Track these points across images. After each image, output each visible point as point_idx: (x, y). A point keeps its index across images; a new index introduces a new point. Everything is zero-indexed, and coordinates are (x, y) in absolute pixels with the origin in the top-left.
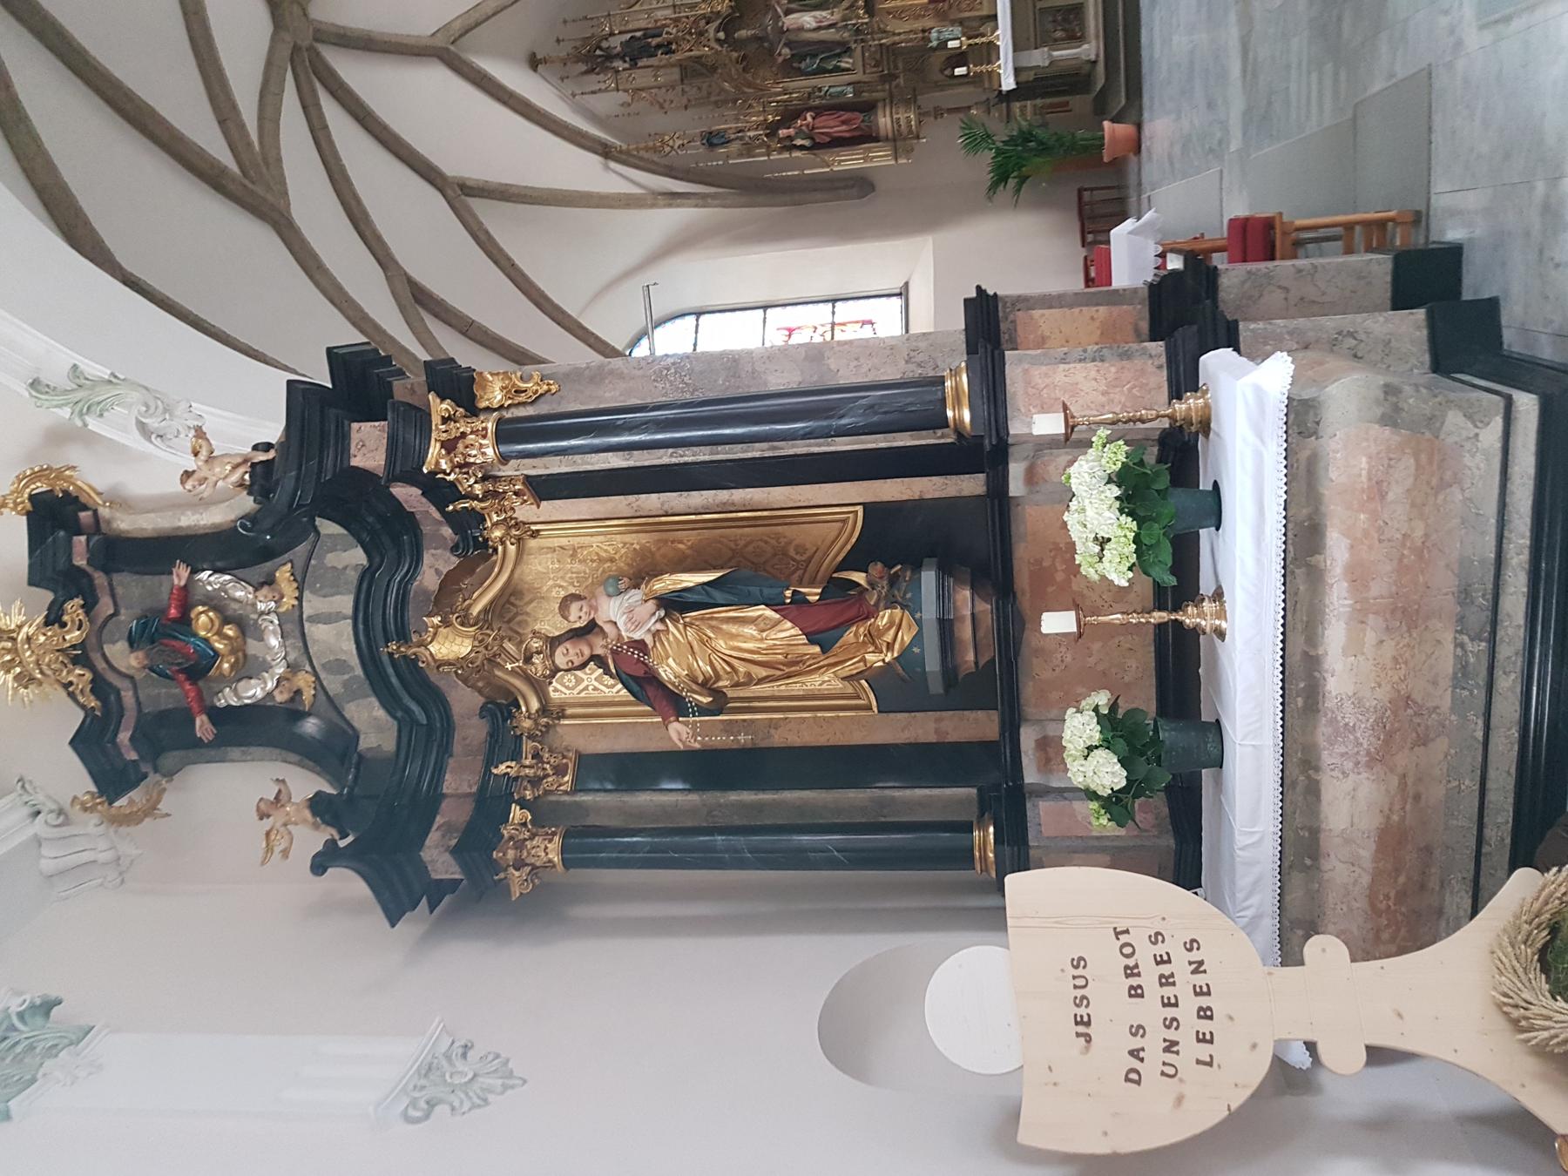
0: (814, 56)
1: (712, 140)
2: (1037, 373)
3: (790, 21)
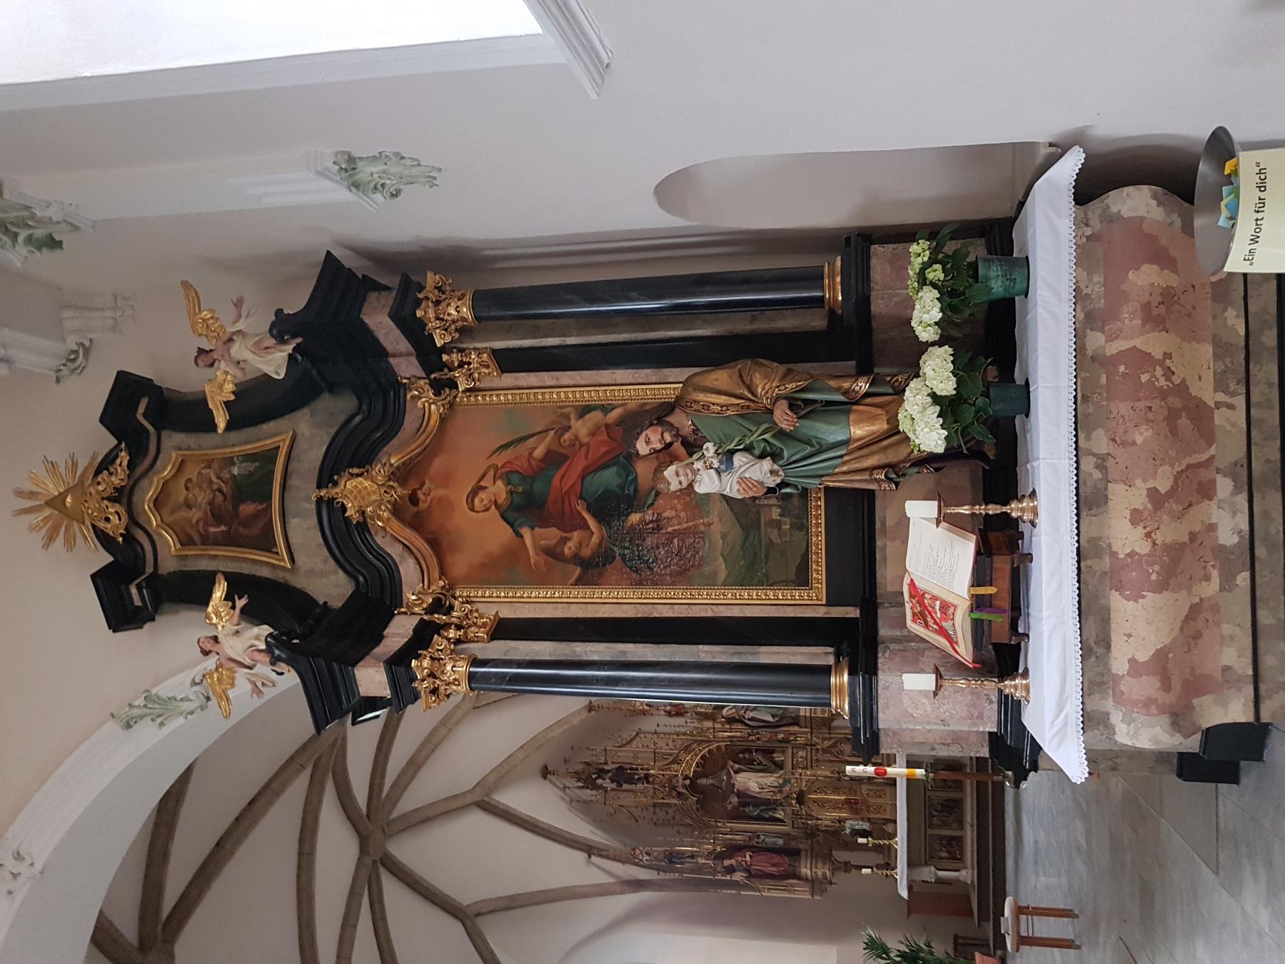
0: (756, 806)
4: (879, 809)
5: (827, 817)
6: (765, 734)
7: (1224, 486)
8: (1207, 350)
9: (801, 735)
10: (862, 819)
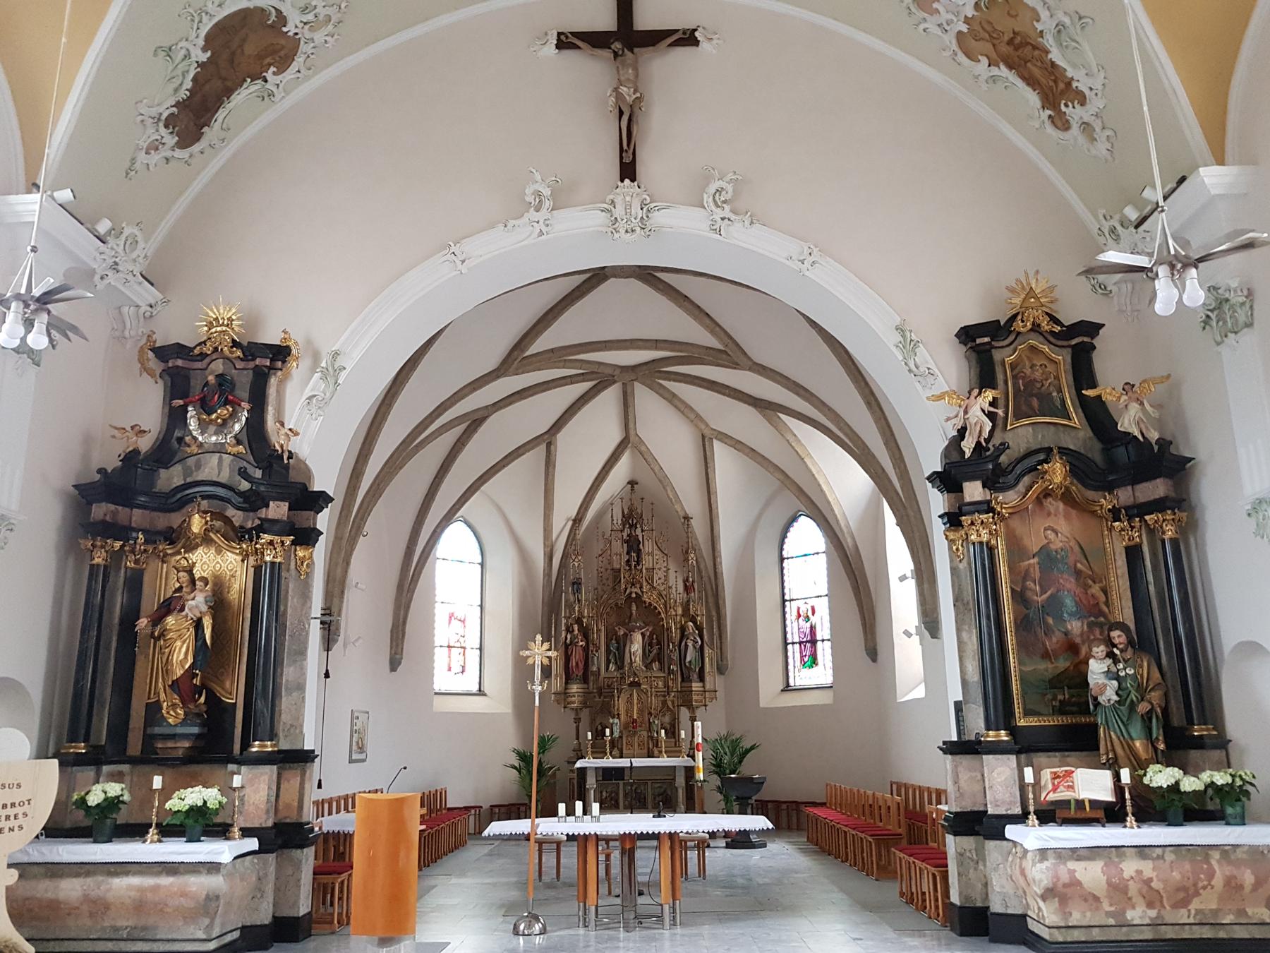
0: (618, 649)
1: (577, 584)
2: (266, 777)
3: (638, 637)
5: (621, 704)
6: (675, 656)
7: (1153, 913)
8: (1214, 907)
9: (676, 684)
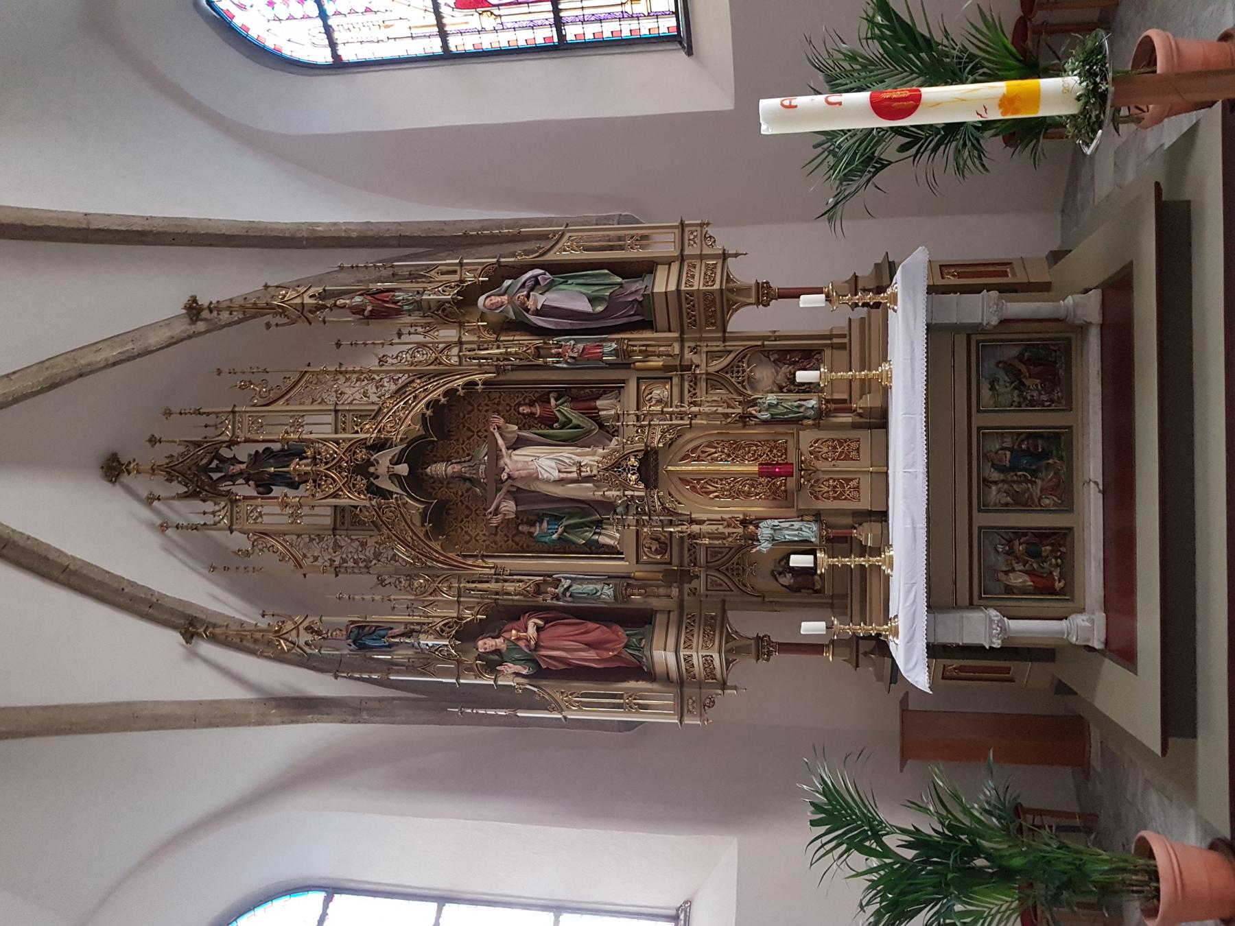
0: (557, 519)
1: (364, 637)
3: (457, 468)
4: (842, 487)
5: (712, 514)
6: (573, 346)
9: (660, 344)
10: (801, 516)
